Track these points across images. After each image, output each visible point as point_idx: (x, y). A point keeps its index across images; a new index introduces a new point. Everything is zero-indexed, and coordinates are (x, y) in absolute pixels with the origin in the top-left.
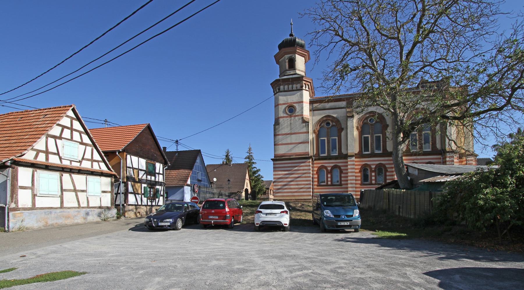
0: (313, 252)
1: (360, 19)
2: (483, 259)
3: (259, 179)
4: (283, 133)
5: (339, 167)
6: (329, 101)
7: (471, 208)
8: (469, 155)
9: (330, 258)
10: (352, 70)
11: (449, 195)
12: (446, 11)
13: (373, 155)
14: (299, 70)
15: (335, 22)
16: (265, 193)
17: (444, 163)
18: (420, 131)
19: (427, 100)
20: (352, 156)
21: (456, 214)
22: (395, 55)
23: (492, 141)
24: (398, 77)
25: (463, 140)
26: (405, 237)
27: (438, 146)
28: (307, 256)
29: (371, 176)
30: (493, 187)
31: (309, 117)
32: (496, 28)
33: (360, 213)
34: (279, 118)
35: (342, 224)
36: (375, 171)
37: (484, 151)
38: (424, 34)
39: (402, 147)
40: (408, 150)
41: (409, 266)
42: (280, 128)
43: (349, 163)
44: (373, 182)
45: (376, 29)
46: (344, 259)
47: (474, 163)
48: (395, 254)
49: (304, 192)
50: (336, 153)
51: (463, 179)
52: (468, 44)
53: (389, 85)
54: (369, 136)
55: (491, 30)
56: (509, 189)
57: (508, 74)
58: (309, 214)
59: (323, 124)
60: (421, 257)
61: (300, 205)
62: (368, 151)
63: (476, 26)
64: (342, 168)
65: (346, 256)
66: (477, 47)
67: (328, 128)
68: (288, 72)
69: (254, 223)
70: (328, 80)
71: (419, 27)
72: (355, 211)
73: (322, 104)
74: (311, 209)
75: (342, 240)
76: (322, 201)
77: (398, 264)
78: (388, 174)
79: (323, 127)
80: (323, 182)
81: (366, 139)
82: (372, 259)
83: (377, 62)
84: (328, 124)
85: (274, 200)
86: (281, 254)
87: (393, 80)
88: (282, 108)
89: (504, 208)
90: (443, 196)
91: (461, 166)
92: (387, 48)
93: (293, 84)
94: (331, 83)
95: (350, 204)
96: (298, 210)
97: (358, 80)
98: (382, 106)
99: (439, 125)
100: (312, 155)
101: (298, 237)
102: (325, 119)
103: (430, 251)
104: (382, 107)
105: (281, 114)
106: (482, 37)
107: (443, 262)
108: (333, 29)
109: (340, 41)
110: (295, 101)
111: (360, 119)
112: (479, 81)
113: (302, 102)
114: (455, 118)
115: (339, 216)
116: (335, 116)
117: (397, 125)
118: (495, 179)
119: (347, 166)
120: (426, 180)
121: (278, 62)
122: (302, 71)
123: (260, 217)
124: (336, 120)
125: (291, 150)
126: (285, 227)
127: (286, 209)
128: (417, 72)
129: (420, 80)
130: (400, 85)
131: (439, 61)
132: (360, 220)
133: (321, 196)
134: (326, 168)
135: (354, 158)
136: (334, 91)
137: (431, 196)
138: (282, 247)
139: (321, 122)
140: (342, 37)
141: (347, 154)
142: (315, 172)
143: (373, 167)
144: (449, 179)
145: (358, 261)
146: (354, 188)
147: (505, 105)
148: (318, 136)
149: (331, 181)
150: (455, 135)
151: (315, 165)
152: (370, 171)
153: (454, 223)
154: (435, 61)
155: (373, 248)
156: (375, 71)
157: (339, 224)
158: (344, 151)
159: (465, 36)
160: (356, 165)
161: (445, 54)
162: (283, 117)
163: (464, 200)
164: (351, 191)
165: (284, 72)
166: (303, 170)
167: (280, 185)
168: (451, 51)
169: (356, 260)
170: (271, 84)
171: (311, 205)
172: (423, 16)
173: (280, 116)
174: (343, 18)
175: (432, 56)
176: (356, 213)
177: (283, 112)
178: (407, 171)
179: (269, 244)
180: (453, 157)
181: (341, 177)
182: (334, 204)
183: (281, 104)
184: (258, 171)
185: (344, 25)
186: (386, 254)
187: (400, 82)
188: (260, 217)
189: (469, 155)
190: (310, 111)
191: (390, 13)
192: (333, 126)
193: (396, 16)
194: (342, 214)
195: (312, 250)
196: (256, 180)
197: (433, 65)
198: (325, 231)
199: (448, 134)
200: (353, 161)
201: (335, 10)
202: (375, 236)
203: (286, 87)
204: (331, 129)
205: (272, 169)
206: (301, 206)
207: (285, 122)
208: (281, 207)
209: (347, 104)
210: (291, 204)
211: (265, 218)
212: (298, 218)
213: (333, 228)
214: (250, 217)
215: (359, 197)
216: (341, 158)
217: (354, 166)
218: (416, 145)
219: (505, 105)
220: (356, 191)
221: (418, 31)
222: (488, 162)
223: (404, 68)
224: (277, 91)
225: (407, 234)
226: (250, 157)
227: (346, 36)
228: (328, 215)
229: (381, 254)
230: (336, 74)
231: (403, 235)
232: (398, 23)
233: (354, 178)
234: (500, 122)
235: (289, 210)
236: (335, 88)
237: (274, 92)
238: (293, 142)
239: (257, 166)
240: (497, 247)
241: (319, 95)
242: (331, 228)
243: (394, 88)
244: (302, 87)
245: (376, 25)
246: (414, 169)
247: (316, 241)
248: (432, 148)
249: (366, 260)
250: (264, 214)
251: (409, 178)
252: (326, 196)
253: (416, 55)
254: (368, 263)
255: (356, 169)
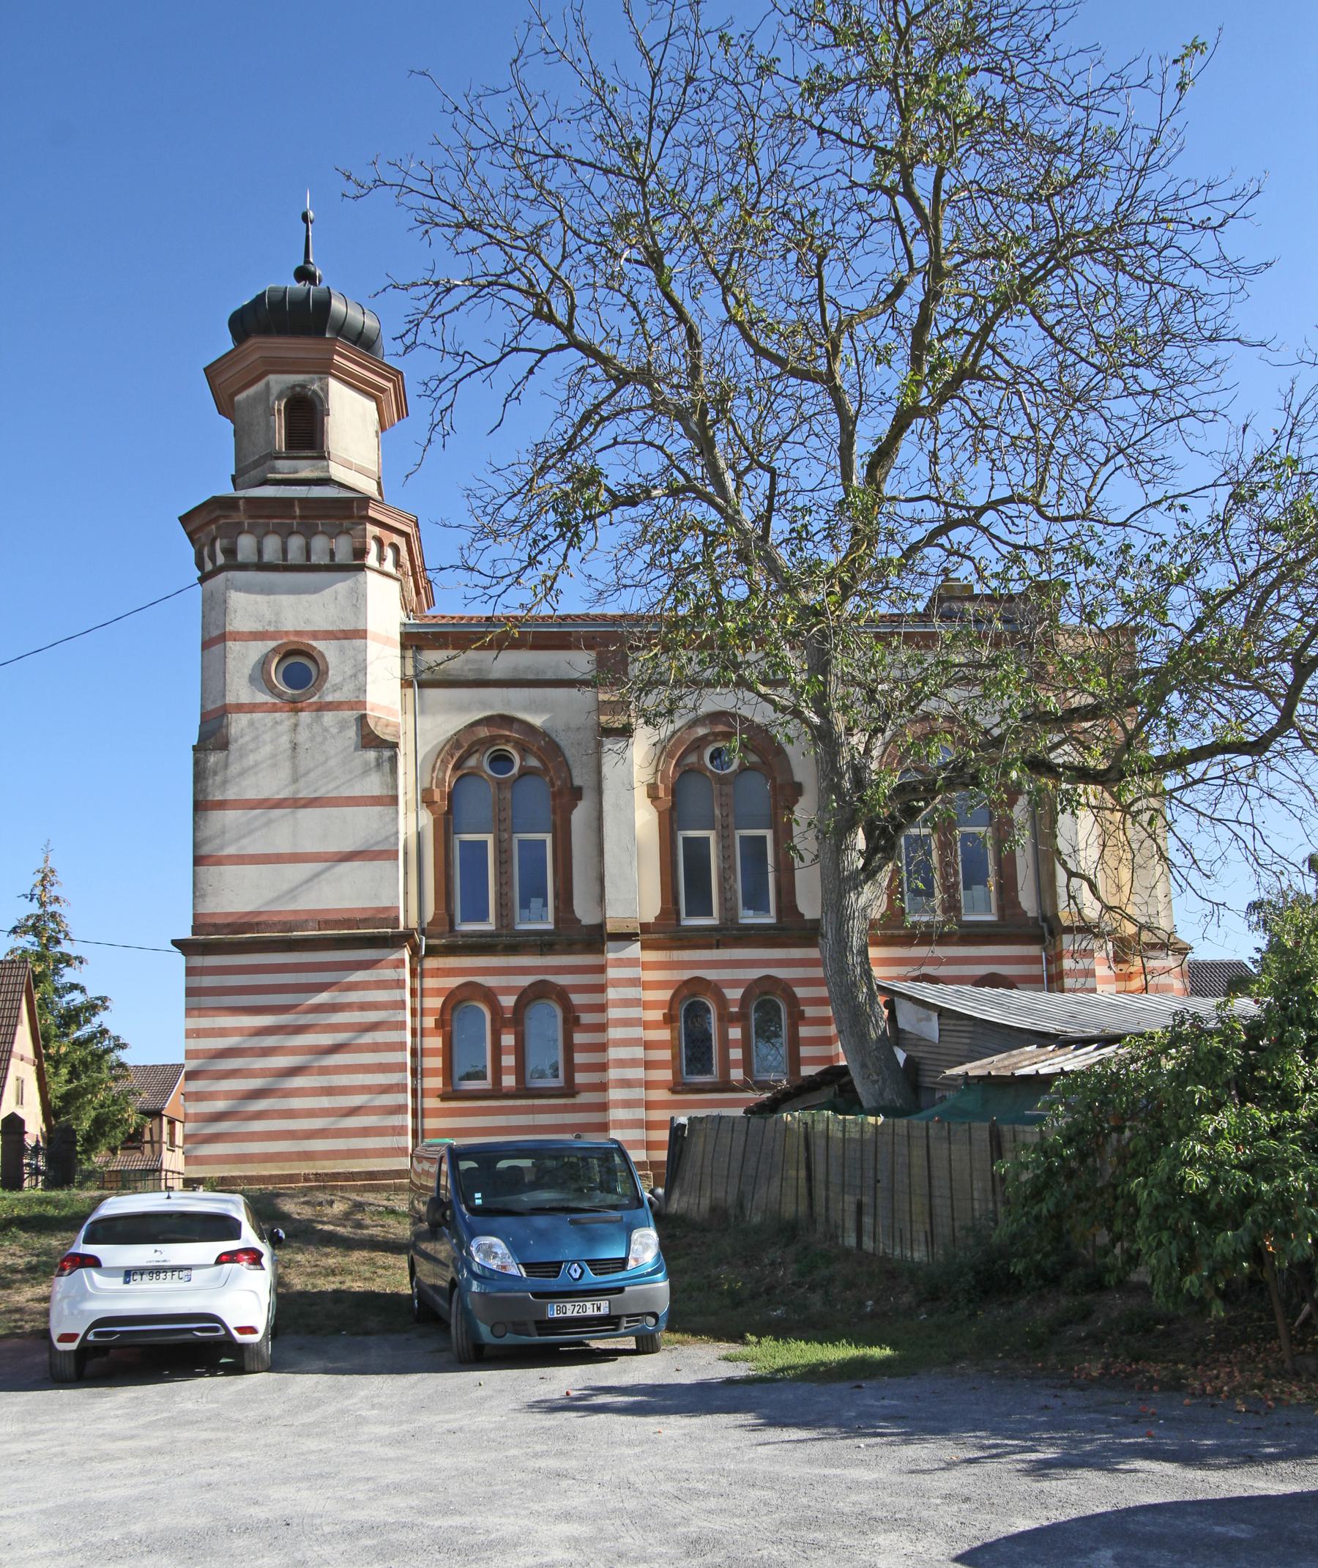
0: (398, 1487)
1: (654, 259)
2: (1214, 1452)
3: (99, 1057)
4: (251, 794)
5: (562, 995)
6: (504, 643)
7: (1157, 1207)
8: (1153, 946)
9: (491, 1520)
10: (617, 501)
11: (1069, 1141)
12: (1025, 292)
13: (731, 935)
14: (348, 465)
15: (531, 251)
16: (134, 1140)
17: (1054, 982)
18: (945, 827)
19: (967, 681)
20: (627, 937)
21: (1103, 1237)
22: (823, 455)
23: (1240, 886)
24: (833, 560)
25: (1125, 874)
26: (885, 1364)
27: (1027, 901)
28: (361, 1515)
29: (726, 1044)
30: (1243, 1104)
31: (399, 719)
32: (1224, 398)
33: (666, 1248)
34: (225, 710)
35: (571, 1309)
36: (741, 1018)
37: (1212, 929)
38: (943, 380)
39: (863, 900)
40: (894, 914)
41: (894, 1523)
42: (234, 769)
43: (612, 973)
44: (737, 1074)
45: (732, 320)
46: (567, 1516)
47: (1177, 984)
48: (828, 1462)
49: (365, 1132)
50: (542, 918)
51: (1123, 1064)
52: (1121, 451)
53: (793, 592)
54: (712, 835)
55: (1209, 402)
56: (1303, 1113)
57: (1279, 600)
58: (390, 1259)
59: (472, 762)
60: (950, 1466)
61: (339, 1208)
62: (709, 913)
63: (1148, 379)
64: (576, 999)
65: (577, 1501)
66: (1157, 469)
67: (499, 784)
68: (280, 464)
69: (46, 1334)
70: (496, 535)
71: (919, 347)
72: (636, 1235)
73: (471, 654)
74: (403, 1230)
75: (570, 1405)
76: (464, 1184)
77: (840, 1520)
78: (804, 1031)
79: (472, 774)
80: (469, 1077)
81: (697, 851)
82: (712, 1503)
83: (739, 476)
84: (501, 760)
85: (190, 1184)
86: (201, 1522)
87: (811, 571)
88: (243, 658)
89: (1284, 1203)
90: (1044, 1149)
91: (1123, 999)
92: (784, 416)
93: (309, 533)
94: (509, 552)
95: (611, 1199)
96: (330, 1240)
97: (645, 553)
98: (763, 689)
99: (1023, 800)
100: (413, 923)
101: (320, 1402)
102: (484, 732)
103: (996, 1431)
104: (765, 698)
105: (240, 689)
106: (1173, 425)
107: (1046, 1485)
108: (523, 284)
109: (560, 348)
110: (322, 624)
111: (663, 750)
112: (1171, 617)
113: (361, 634)
114: (1084, 775)
115: (554, 1268)
116: (537, 720)
117: (836, 788)
118: (1250, 1066)
119: (601, 989)
120: (975, 1068)
121: (225, 406)
122: (361, 471)
123: (85, 1296)
124: (544, 745)
125: (293, 892)
126: (243, 1347)
127: (249, 1237)
128: (914, 548)
129: (932, 582)
130: (845, 598)
131: (1011, 509)
132: (662, 1285)
133: (456, 1155)
134: (489, 996)
135: (634, 950)
136: (527, 597)
137: (997, 1150)
138: (215, 1475)
139: (461, 748)
140: (568, 329)
141: (601, 926)
142: (430, 1022)
143: (734, 994)
144: (1073, 1061)
145: (642, 1519)
146: (636, 1109)
147: (1274, 733)
148: (447, 825)
149: (520, 1069)
150: (1094, 853)
151: (430, 983)
152: (721, 1018)
153: (1096, 1284)
154: (992, 505)
155: (724, 1438)
156: (731, 518)
157: (554, 1311)
158: (584, 912)
159: (1106, 413)
160: (647, 986)
161: (1030, 481)
162: (252, 708)
163: (1131, 1164)
164: (623, 1125)
165: (256, 464)
166: (364, 1007)
167: (228, 1095)
168: (1054, 470)
169: (631, 1515)
170: (184, 520)
171: (404, 1208)
172: (933, 295)
173: (231, 699)
174: (573, 243)
175: (979, 484)
176: (645, 1246)
177: (252, 679)
178: (892, 1018)
179: (134, 1463)
180: (1088, 953)
181: (569, 1048)
182: (527, 1199)
183: (238, 636)
184: (93, 1008)
185: (578, 273)
186: (788, 1471)
187: (846, 588)
188: (85, 1296)
189: (1153, 946)
190: (406, 683)
191: (792, 257)
192: (525, 772)
193: (819, 276)
194: (567, 1253)
195: (392, 1477)
196: (77, 1055)
197: (984, 520)
198: (480, 1356)
199: (1062, 844)
200: (632, 963)
201: (532, 193)
202: (740, 1370)
203: (272, 545)
204: (512, 792)
205: (180, 1000)
206: (347, 1215)
207: (263, 742)
208: (221, 1227)
209: (601, 663)
210: (289, 1207)
211: (116, 1295)
212: (328, 1285)
213: (524, 1337)
214: (24, 1295)
215: (662, 1155)
216: (569, 948)
217: (636, 991)
218: (930, 894)
219: (1274, 733)
220: (649, 1125)
221: (916, 361)
222: (1234, 980)
223: (861, 514)
224: (221, 559)
225: (894, 1346)
226: (44, 927)
227: (586, 330)
228: (494, 1264)
229: (762, 1467)
230: (541, 510)
231: (877, 1352)
232: (830, 308)
233: (639, 1052)
234: (1265, 801)
235: (275, 1242)
236: (532, 577)
237: (200, 564)
238: (308, 847)
239: (90, 978)
240: (1277, 1386)
241: (455, 602)
242: (510, 1339)
243: (817, 613)
244: (361, 553)
245: (731, 301)
246: (923, 1012)
247: (425, 1419)
248: (1001, 909)
249: (681, 1509)
250: (112, 1272)
251: (901, 1056)
252: (486, 1155)
253: (913, 469)
254: (692, 1530)
255: (647, 1005)
